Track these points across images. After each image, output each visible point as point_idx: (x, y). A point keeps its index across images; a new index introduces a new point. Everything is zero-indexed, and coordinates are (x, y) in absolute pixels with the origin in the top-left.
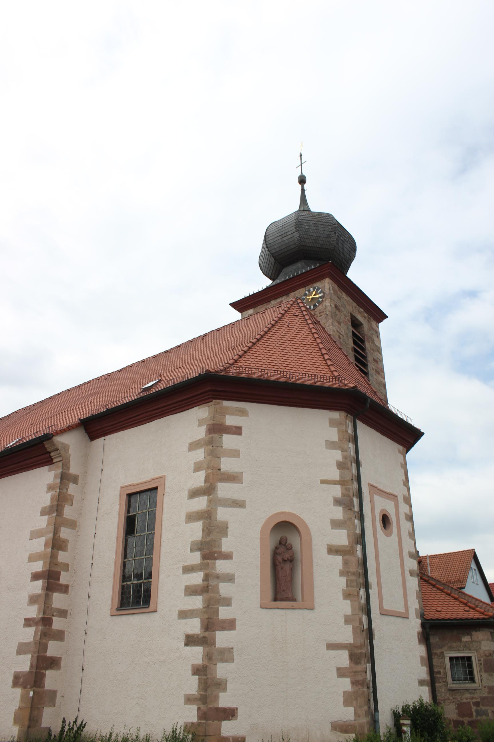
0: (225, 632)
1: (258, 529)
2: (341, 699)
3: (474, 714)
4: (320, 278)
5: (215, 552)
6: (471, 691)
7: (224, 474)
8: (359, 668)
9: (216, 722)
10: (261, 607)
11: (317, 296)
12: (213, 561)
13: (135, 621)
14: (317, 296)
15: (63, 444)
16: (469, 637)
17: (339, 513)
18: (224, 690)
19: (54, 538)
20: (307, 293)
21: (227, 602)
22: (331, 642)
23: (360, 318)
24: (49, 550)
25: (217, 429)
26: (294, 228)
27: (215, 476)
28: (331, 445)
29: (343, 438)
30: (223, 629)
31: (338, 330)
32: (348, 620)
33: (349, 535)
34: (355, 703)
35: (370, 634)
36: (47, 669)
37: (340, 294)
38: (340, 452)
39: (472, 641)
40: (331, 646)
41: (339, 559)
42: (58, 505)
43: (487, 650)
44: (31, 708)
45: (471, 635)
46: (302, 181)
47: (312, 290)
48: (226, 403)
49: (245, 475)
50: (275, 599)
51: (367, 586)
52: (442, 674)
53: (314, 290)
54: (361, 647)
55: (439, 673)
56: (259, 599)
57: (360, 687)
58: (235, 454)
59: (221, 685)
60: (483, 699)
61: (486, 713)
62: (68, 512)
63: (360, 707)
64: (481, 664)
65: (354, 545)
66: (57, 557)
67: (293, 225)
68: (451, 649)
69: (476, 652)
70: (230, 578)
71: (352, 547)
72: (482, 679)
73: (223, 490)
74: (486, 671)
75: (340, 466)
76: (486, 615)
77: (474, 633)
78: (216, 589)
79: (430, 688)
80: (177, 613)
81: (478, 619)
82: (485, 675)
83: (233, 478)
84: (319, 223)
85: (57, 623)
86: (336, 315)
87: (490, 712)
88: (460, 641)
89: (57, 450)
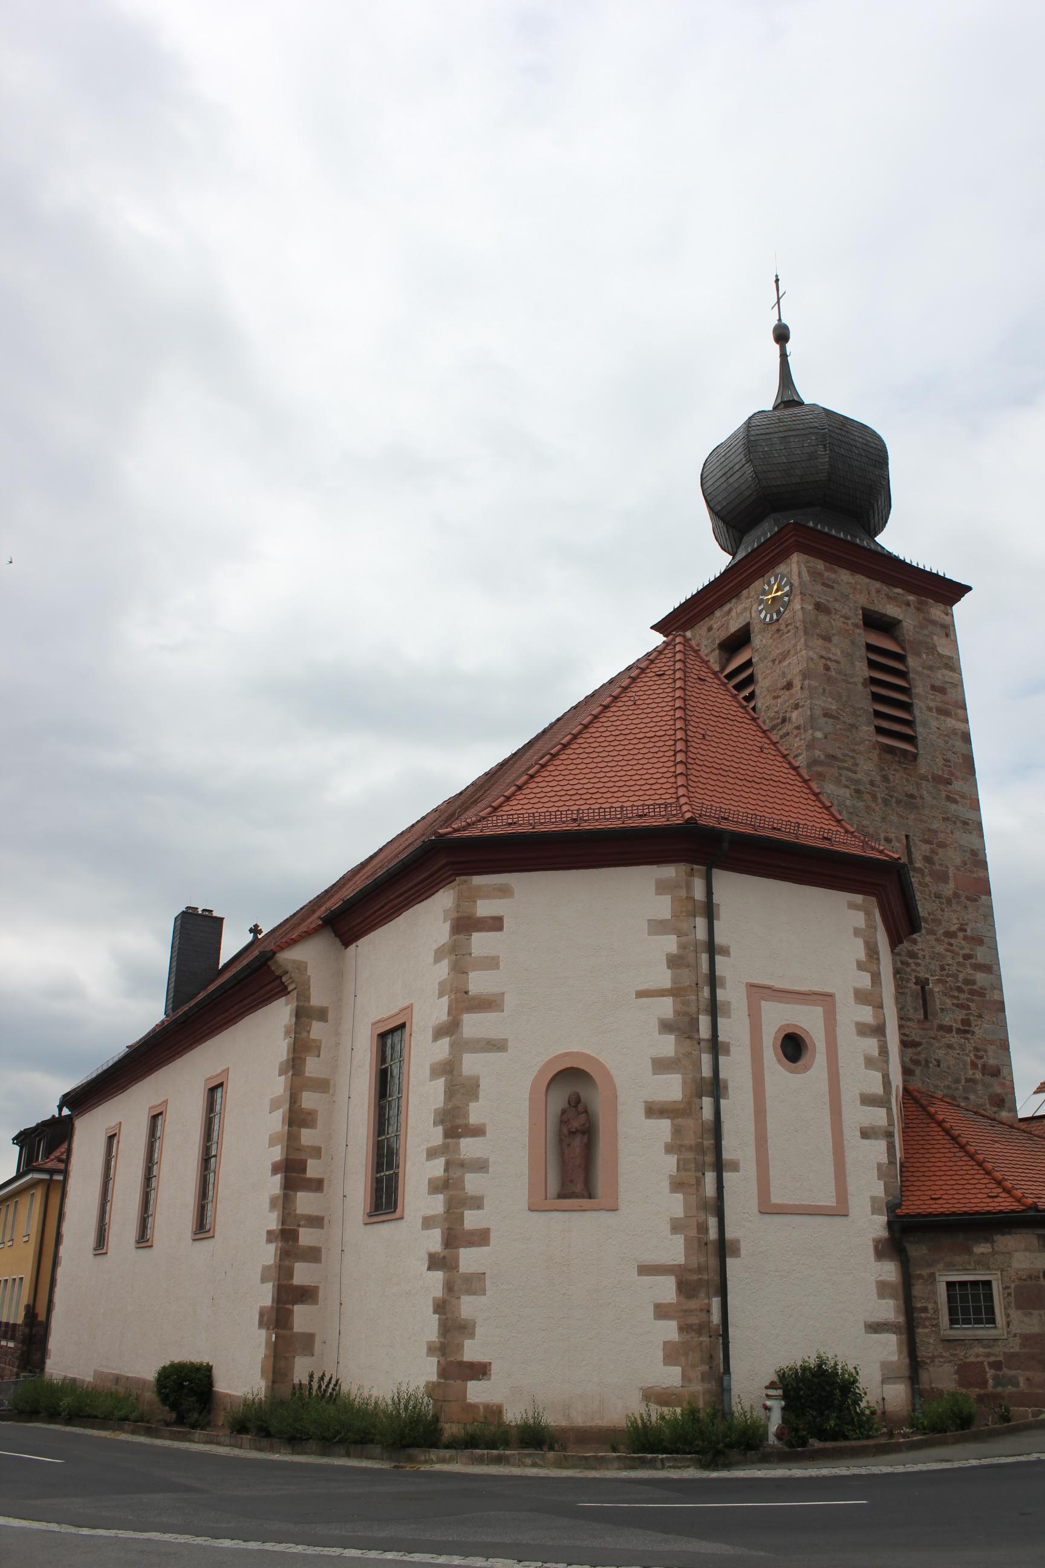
0: (473, 1249)
1: (527, 1084)
2: (660, 1354)
3: (990, 1382)
4: (782, 556)
5: (458, 1126)
6: (985, 1342)
7: (474, 998)
8: (693, 1304)
9: (459, 1382)
10: (530, 1210)
11: (779, 593)
12: (455, 1140)
13: (385, 1230)
14: (779, 593)
15: (294, 962)
16: (989, 1245)
17: (667, 1045)
18: (472, 1335)
19: (291, 1110)
20: (766, 587)
21: (477, 1203)
22: (645, 1263)
23: (892, 610)
24: (286, 1127)
25: (465, 925)
26: (742, 456)
27: (464, 1002)
28: (658, 927)
29: (682, 912)
30: (470, 1244)
31: (824, 653)
32: (676, 1226)
33: (684, 1083)
34: (683, 1359)
35: (723, 1249)
36: (294, 1303)
37: (833, 576)
38: (674, 938)
39: (994, 1253)
40: (645, 1270)
41: (665, 1126)
42: (294, 1059)
43: (1023, 1269)
44: (275, 1357)
45: (992, 1242)
46: (782, 335)
47: (772, 580)
48: (478, 880)
49: (507, 998)
50: (561, 1196)
51: (719, 1166)
52: (931, 1311)
53: (776, 581)
54: (700, 1269)
55: (925, 1310)
56: (526, 1197)
57: (694, 1334)
58: (492, 963)
59: (466, 1329)
60: (1010, 1357)
61: (1013, 1381)
62: (313, 1067)
63: (693, 1366)
64: (1009, 1294)
65: (697, 1100)
66: (300, 1139)
67: (740, 450)
68: (950, 1267)
69: (999, 1273)
70: (481, 1166)
71: (689, 1103)
72: (1010, 1323)
73: (473, 1025)
74: (1019, 1307)
75: (674, 962)
76: (1023, 1205)
77: (999, 1238)
78: (460, 1184)
79: (904, 1337)
80: (421, 1220)
81: (1013, 1211)
82: (1015, 1314)
83: (488, 1004)
84: (791, 433)
85: (307, 1237)
86: (816, 624)
87: (1021, 1380)
88: (970, 1252)
89: (287, 972)
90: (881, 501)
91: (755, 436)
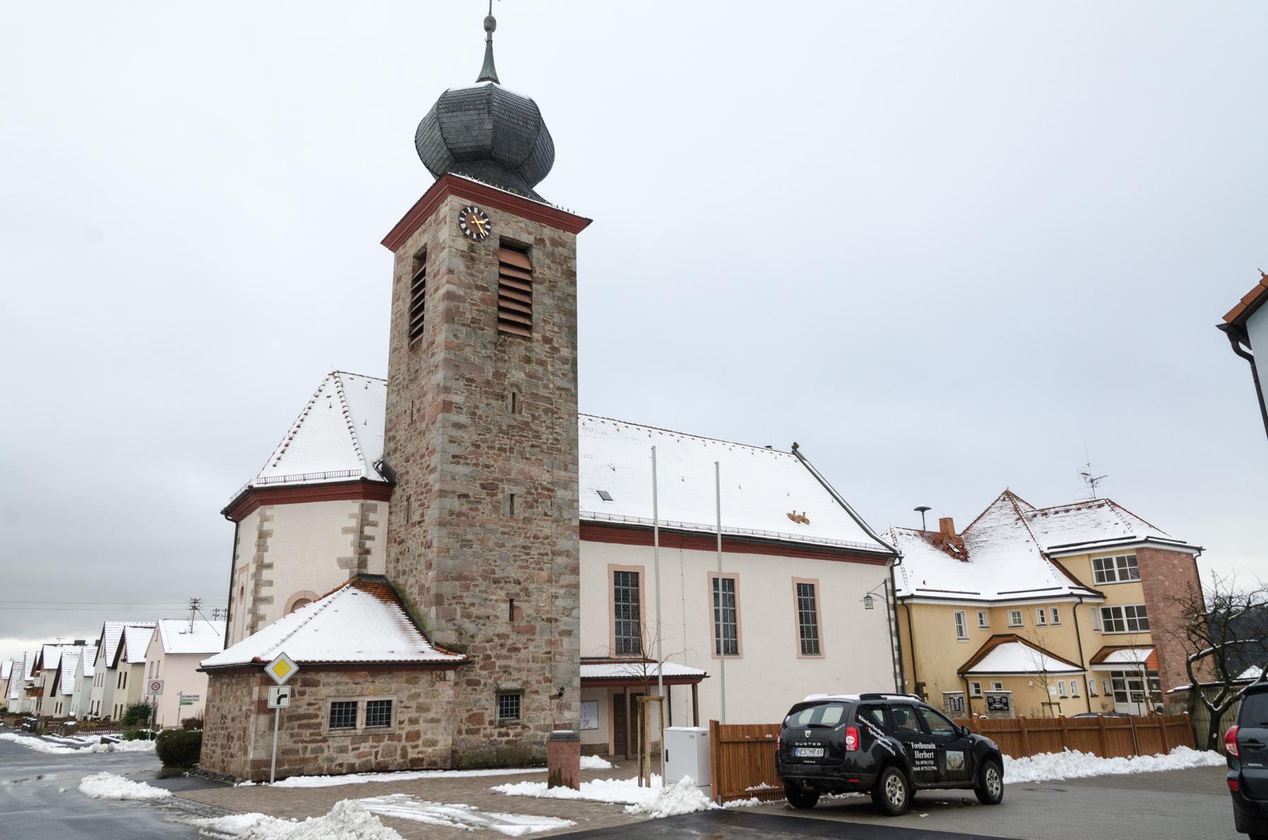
70: (270, 583)
91: (450, 104)
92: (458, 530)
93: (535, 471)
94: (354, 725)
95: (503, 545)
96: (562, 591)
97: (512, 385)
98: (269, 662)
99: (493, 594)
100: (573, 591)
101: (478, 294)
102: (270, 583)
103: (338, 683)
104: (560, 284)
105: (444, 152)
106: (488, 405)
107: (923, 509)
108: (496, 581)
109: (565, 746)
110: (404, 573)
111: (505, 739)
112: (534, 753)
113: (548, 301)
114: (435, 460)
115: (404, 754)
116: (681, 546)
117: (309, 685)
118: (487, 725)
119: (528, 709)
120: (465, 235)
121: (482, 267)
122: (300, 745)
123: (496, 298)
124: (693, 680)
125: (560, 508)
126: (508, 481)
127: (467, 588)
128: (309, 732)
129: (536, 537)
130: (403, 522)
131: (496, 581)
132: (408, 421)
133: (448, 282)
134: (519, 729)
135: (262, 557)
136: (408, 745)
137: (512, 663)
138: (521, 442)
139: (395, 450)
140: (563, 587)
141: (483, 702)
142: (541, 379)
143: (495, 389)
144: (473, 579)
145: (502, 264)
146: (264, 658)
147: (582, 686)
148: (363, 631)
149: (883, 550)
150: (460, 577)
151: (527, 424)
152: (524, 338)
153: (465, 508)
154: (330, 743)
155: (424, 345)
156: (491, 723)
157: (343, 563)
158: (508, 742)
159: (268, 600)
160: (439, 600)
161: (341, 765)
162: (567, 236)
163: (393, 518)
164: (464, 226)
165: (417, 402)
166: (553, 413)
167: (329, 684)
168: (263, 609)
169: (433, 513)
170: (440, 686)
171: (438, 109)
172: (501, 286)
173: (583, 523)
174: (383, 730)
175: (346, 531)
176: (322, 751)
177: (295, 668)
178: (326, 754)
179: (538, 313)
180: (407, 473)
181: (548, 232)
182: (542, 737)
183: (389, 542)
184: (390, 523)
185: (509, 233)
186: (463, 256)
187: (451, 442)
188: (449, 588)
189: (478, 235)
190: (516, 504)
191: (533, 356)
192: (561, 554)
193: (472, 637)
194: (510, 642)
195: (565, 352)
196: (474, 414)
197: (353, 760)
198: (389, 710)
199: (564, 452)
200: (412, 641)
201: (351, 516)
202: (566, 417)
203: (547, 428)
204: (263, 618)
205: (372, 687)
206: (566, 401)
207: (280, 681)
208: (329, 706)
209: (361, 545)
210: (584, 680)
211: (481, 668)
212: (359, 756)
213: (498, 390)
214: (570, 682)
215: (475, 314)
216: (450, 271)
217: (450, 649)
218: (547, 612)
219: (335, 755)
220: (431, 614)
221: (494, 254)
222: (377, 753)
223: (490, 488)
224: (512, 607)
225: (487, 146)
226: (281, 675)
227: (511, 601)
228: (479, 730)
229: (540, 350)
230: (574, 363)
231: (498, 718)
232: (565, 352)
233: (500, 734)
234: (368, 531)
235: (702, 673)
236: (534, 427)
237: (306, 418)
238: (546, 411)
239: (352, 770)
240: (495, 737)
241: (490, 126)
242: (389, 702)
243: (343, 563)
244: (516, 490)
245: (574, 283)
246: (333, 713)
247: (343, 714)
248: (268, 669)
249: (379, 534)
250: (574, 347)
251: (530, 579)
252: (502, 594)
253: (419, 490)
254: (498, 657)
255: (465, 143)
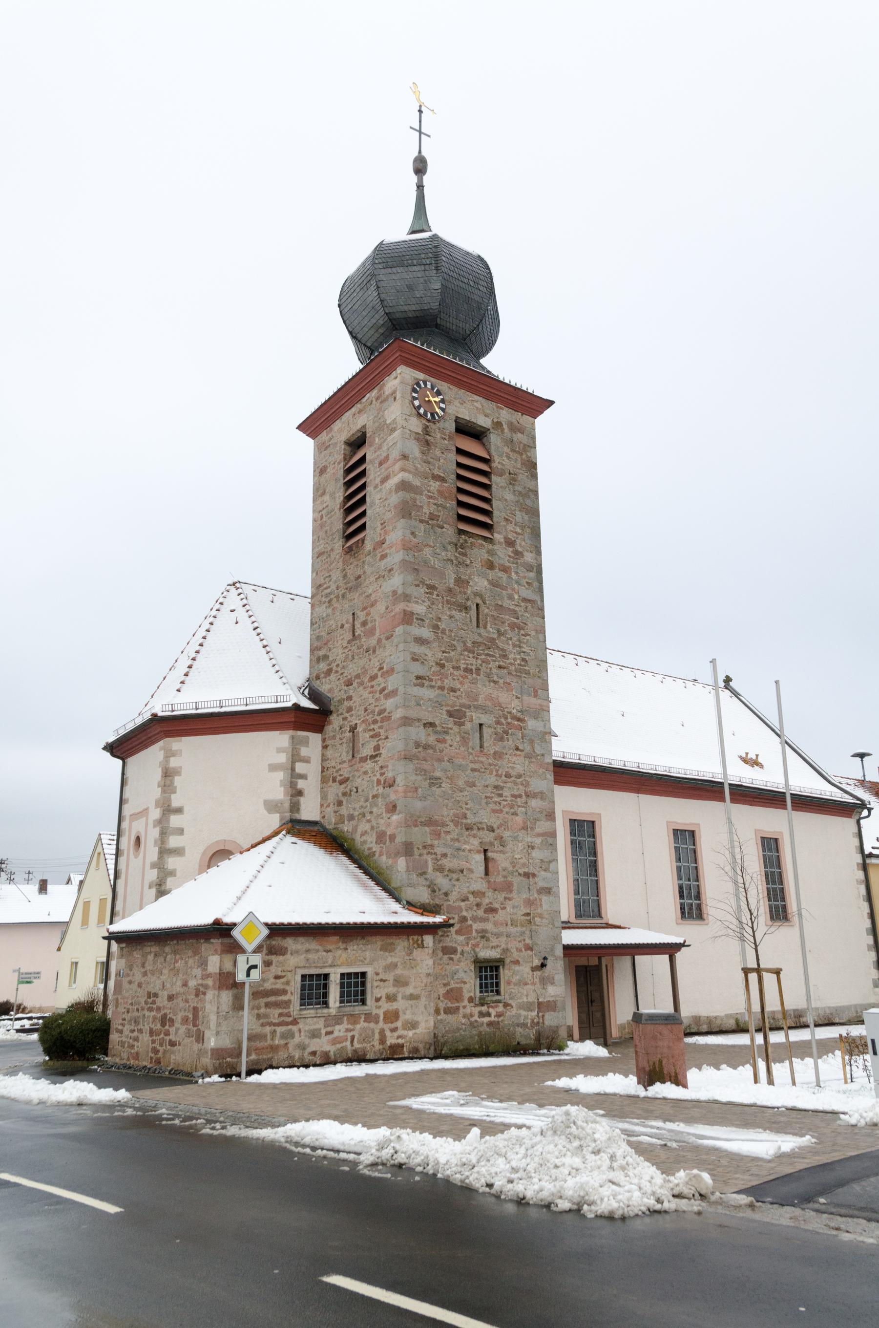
46: (420, 167)
70: (181, 831)
90: (487, 321)
91: (386, 258)
92: (426, 766)
93: (504, 697)
94: (326, 1004)
95: (473, 785)
96: (538, 841)
97: (476, 594)
98: (235, 925)
99: (466, 842)
100: (550, 840)
101: (435, 485)
102: (181, 831)
103: (308, 951)
104: (520, 477)
105: (380, 318)
106: (451, 617)
107: (862, 756)
108: (468, 828)
109: (664, 1029)
110: (351, 818)
111: (486, 1020)
112: (518, 1038)
113: (510, 497)
114: (392, 682)
115: (382, 1041)
116: (638, 791)
117: (276, 954)
118: (466, 1002)
119: (509, 983)
120: (419, 414)
121: (438, 453)
122: (268, 1029)
123: (455, 490)
124: (671, 950)
125: (532, 742)
126: (477, 708)
127: (438, 835)
128: (277, 1011)
129: (508, 776)
130: (347, 757)
131: (468, 828)
132: (349, 636)
133: (403, 470)
134: (501, 1008)
135: (170, 800)
136: (387, 1027)
137: (489, 926)
138: (488, 663)
139: (329, 672)
140: (539, 835)
141: (461, 975)
142: (504, 588)
143: (457, 598)
144: (444, 825)
145: (460, 451)
146: (227, 920)
147: (565, 955)
148: (323, 891)
149: (850, 800)
150: (430, 822)
151: (492, 640)
152: (485, 538)
153: (432, 739)
154: (301, 1026)
155: (368, 546)
156: (471, 1000)
157: (271, 806)
158: (490, 1024)
159: (179, 852)
160: (408, 849)
161: (314, 1053)
162: (525, 419)
163: (329, 753)
164: (417, 403)
165: (361, 616)
166: (520, 628)
167: (297, 952)
168: (172, 862)
169: (395, 743)
170: (417, 953)
171: (374, 264)
172: (459, 477)
173: (554, 761)
174: (358, 1009)
175: (273, 768)
176: (293, 1036)
177: (265, 932)
178: (297, 1040)
179: (499, 513)
180: (350, 698)
181: (505, 415)
182: (526, 1018)
183: (324, 780)
184: (324, 759)
185: (466, 414)
186: (418, 439)
187: (414, 660)
188: (420, 835)
189: (432, 415)
190: (486, 736)
191: (496, 561)
192: (534, 795)
193: (446, 894)
194: (486, 901)
195: (529, 557)
196: (436, 627)
197: (326, 1048)
198: (363, 984)
199: (532, 674)
200: (379, 899)
201: (279, 750)
202: (533, 633)
203: (514, 646)
204: (172, 873)
205: (344, 955)
206: (532, 615)
207: (249, 947)
208: (299, 978)
209: (293, 785)
210: (567, 948)
211: (457, 932)
212: (334, 1042)
213: (460, 599)
214: (552, 949)
215: (433, 508)
216: (405, 457)
217: (424, 909)
218: (524, 865)
219: (307, 1041)
220: (399, 869)
221: (450, 438)
222: (353, 1038)
223: (457, 715)
224: (486, 859)
225: (424, 313)
226: (250, 939)
227: (485, 851)
228: (458, 1008)
229: (503, 554)
230: (539, 572)
231: (478, 994)
232: (529, 557)
233: (482, 1014)
234: (300, 768)
235: (680, 940)
236: (500, 645)
237: (209, 635)
238: (513, 626)
239: (327, 1061)
240: (476, 1018)
241: (437, 286)
242: (363, 974)
243: (271, 806)
244: (485, 719)
245: (534, 476)
246: (303, 988)
247: (314, 989)
248: (235, 933)
249: (311, 770)
250: (538, 552)
251: (504, 825)
252: (476, 842)
253: (370, 718)
254: (475, 919)
255: (408, 306)
